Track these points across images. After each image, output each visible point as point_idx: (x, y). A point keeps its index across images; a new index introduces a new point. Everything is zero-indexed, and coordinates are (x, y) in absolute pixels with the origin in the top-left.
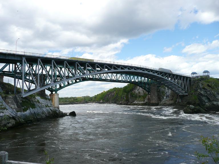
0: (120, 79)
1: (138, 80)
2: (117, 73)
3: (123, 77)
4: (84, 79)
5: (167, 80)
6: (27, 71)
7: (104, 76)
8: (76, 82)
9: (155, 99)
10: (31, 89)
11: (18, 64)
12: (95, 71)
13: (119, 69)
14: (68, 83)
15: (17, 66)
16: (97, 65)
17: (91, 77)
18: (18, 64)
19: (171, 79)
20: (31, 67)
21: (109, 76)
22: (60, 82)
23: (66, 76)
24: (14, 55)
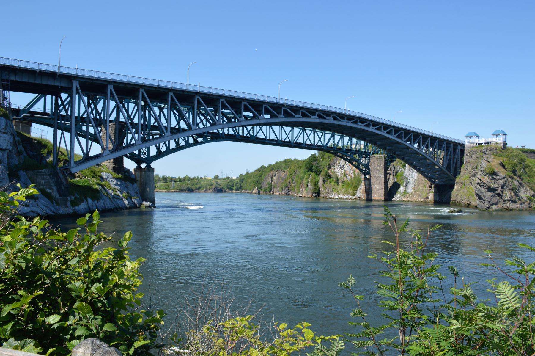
0: (300, 140)
1: (343, 143)
2: (292, 125)
3: (308, 137)
4: (216, 137)
5: (409, 148)
6: (84, 113)
7: (263, 132)
8: (196, 143)
9: (378, 190)
10: (91, 154)
11: (64, 96)
12: (241, 119)
13: (296, 116)
14: (177, 144)
15: (60, 103)
16: (245, 105)
17: (231, 132)
18: (64, 96)
19: (419, 145)
20: (93, 106)
21: (276, 132)
22: (158, 140)
23: (172, 128)
24: (53, 75)
